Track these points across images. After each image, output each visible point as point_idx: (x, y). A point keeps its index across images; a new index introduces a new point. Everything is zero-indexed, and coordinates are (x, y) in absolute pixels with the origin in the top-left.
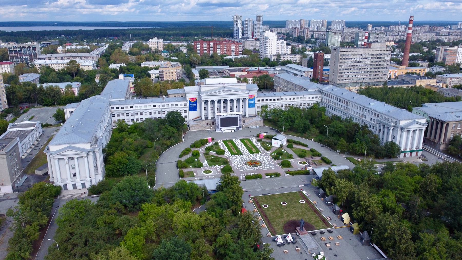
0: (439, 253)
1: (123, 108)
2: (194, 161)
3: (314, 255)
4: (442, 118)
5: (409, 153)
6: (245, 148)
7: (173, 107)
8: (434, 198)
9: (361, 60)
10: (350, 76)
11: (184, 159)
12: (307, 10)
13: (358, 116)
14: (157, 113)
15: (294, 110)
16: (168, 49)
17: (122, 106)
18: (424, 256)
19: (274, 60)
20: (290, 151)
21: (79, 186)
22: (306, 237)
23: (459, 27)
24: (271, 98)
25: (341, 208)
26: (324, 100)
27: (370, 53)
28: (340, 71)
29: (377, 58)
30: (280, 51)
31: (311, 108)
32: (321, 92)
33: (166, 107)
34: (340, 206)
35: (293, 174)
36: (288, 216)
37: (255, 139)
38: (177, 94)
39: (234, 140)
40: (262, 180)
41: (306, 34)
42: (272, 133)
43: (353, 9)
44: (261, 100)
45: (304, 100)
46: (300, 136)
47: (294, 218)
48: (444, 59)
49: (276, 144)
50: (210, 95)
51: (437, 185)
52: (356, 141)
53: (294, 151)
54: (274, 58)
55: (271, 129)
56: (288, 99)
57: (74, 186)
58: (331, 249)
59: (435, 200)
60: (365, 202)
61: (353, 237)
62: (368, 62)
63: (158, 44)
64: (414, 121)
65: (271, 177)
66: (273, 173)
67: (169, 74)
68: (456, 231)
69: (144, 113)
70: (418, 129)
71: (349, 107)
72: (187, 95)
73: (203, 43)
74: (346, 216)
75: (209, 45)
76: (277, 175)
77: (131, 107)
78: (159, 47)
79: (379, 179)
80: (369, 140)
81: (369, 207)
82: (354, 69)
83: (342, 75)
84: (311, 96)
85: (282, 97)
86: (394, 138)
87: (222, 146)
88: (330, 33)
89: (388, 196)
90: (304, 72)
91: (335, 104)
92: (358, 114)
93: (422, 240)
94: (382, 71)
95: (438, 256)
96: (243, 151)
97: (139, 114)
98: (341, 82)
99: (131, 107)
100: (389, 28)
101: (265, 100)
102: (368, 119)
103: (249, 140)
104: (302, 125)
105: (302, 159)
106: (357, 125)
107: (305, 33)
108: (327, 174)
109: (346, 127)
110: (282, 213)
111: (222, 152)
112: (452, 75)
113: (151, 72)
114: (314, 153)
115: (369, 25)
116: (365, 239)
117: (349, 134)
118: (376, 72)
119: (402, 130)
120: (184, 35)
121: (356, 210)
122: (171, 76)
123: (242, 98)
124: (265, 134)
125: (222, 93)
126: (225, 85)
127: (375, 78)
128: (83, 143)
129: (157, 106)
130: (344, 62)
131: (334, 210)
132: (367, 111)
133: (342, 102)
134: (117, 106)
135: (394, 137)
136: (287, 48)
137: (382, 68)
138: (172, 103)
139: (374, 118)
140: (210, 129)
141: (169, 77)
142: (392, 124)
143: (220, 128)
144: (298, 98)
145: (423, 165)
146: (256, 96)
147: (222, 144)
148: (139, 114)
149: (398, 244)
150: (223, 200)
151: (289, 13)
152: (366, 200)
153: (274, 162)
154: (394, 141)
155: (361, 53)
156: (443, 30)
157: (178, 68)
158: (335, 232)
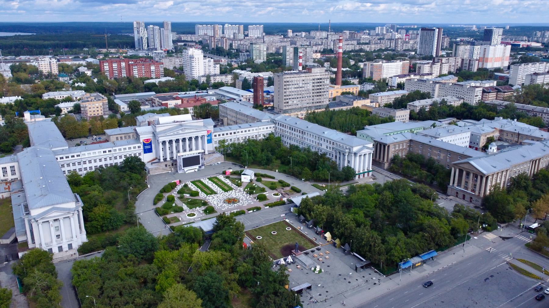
0: (401, 249)
1: (68, 157)
2: (172, 207)
3: (313, 269)
4: (384, 141)
5: (362, 175)
6: (217, 187)
7: (125, 151)
8: (390, 210)
9: (303, 86)
10: (295, 102)
11: (160, 204)
12: (218, 9)
13: (314, 144)
14: (108, 159)
15: (251, 143)
16: (63, 69)
17: (67, 155)
18: (392, 253)
19: (203, 82)
20: (261, 185)
21: (65, 247)
22: (302, 257)
23: (377, 32)
24: (227, 132)
25: (322, 229)
26: (277, 130)
27: (311, 78)
28: (285, 98)
29: (318, 82)
30: (208, 71)
31: (267, 139)
32: (273, 122)
33: (118, 151)
34: (321, 228)
35: (272, 205)
36: (281, 242)
37: (223, 177)
38: (120, 134)
39: (202, 180)
40: (246, 216)
41: (225, 44)
42: (238, 169)
43: (270, 9)
44: (217, 135)
45: (259, 131)
46: (264, 169)
47: (287, 244)
48: (372, 73)
49: (245, 179)
50: (168, 135)
51: (391, 200)
52: (318, 169)
53: (264, 184)
54: (203, 80)
55: (233, 164)
56: (244, 132)
57: (60, 249)
58: (323, 262)
59: (390, 212)
60: (343, 220)
61: (337, 250)
62: (310, 87)
63: (50, 66)
64: (364, 146)
65: (253, 211)
66: (255, 207)
67: (94, 109)
68: (408, 233)
69: (93, 161)
70: (367, 153)
71: (304, 136)
72: (141, 137)
73: (112, 63)
74: (328, 235)
75: (119, 66)
76: (258, 209)
77: (78, 156)
78: (53, 69)
79: (346, 200)
80: (330, 167)
81: (347, 224)
82: (298, 95)
83: (287, 101)
84: (265, 127)
85: (238, 131)
86: (349, 163)
87: (194, 188)
88: (254, 46)
89: (358, 214)
90: (242, 96)
91: (290, 134)
92: (314, 142)
93: (388, 243)
94: (323, 95)
95: (401, 251)
96: (216, 191)
97: (87, 162)
98: (287, 108)
99: (78, 156)
100: (310, 33)
101: (221, 135)
102: (324, 147)
103: (216, 178)
104: (265, 158)
105: (274, 191)
106: (316, 153)
107: (223, 43)
108: (304, 201)
109: (308, 156)
110: (275, 242)
111: (197, 194)
112: (382, 94)
113: (61, 105)
114: (283, 184)
115: (289, 31)
116: (347, 250)
117: (311, 163)
118: (318, 96)
119: (355, 155)
120: (66, 46)
121: (336, 228)
122: (96, 111)
123: (201, 135)
124: (231, 171)
125: (181, 132)
126: (182, 123)
127: (318, 102)
128: (68, 202)
129: (107, 152)
130: (288, 89)
131: (317, 231)
132: (323, 139)
133: (297, 132)
134: (61, 156)
135: (349, 162)
136: (215, 67)
137: (323, 92)
138: (125, 147)
139: (329, 145)
140: (171, 170)
141: (98, 112)
142: (347, 151)
143: (183, 168)
144: (253, 130)
145: (375, 184)
146: (213, 131)
147: (192, 185)
148: (87, 162)
149: (373, 248)
150: (229, 237)
151: (195, 13)
152: (344, 218)
153: (250, 197)
154: (349, 165)
155: (304, 78)
156: (363, 36)
157: (104, 102)
158: (322, 249)
